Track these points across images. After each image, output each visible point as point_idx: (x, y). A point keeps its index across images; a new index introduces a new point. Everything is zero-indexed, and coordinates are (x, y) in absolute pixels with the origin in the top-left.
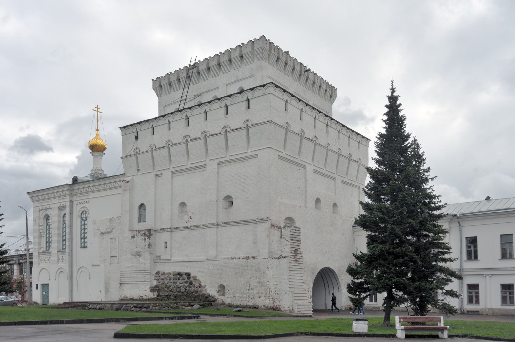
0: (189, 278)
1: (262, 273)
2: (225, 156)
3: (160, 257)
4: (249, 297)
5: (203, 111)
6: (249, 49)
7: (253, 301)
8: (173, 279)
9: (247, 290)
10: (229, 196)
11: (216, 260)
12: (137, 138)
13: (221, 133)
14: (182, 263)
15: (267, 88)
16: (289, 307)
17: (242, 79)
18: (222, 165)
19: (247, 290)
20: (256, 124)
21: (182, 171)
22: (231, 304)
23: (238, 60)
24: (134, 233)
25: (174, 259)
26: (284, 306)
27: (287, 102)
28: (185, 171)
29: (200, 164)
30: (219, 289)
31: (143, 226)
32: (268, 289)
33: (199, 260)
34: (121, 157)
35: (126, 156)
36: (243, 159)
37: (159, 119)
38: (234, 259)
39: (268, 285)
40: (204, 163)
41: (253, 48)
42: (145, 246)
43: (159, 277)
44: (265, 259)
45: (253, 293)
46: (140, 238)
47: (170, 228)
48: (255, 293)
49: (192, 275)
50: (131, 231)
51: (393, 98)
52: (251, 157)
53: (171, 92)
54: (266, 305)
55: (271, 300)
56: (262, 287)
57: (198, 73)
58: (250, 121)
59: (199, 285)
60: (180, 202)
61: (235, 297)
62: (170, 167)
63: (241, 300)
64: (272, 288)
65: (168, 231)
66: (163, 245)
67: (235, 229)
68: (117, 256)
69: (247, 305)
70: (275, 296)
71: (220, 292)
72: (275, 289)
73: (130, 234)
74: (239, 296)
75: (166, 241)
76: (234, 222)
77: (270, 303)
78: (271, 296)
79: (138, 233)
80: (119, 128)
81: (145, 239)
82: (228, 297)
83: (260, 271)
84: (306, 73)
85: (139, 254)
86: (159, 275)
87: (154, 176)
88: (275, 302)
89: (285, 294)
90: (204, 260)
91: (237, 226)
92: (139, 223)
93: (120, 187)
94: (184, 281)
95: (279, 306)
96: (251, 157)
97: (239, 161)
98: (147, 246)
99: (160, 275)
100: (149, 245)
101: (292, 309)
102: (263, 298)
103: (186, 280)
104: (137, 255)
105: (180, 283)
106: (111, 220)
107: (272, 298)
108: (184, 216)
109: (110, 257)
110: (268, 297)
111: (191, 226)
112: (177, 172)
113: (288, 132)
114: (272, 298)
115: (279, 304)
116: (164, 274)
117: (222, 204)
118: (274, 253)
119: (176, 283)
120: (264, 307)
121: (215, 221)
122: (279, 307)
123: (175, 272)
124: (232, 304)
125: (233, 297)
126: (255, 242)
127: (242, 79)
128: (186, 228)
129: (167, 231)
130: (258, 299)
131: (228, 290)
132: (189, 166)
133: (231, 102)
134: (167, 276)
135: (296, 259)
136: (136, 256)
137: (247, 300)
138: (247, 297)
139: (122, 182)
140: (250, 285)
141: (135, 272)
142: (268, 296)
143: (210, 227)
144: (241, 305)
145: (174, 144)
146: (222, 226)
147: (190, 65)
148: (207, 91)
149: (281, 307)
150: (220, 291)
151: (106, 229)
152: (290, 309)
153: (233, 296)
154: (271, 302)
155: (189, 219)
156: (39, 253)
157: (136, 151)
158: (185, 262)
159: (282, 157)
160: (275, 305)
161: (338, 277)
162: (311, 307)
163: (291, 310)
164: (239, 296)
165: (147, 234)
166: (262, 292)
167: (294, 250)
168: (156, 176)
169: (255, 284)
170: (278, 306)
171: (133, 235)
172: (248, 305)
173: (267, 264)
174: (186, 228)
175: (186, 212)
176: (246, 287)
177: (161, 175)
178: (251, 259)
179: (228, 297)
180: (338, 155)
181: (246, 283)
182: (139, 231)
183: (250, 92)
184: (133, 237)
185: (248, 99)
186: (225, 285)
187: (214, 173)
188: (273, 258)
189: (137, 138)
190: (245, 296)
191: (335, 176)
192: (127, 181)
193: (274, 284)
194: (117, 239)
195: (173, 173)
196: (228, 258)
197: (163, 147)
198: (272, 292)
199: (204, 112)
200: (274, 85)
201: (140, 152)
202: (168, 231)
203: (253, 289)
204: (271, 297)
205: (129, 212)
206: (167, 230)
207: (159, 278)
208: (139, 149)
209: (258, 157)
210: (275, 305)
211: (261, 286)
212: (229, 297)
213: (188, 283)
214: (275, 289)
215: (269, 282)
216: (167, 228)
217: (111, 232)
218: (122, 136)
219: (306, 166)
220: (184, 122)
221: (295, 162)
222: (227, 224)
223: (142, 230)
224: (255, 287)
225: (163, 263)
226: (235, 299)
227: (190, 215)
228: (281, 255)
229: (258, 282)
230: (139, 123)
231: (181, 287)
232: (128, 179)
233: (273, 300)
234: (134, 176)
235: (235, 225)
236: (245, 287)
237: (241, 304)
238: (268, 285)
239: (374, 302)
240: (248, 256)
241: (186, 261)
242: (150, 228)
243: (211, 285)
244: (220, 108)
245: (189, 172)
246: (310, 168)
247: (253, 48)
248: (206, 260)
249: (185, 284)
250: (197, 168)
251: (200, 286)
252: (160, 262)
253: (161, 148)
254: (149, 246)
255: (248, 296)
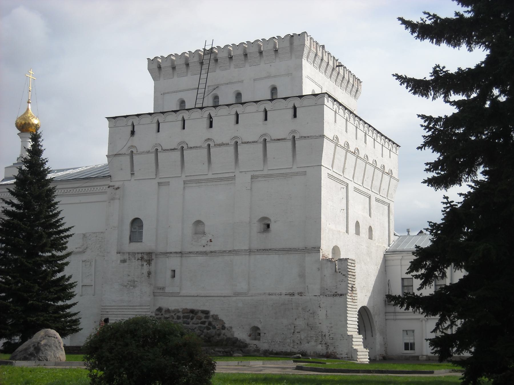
0: (207, 317)
1: (311, 313)
2: (291, 167)
3: (163, 288)
4: (293, 342)
5: (291, 106)
6: (287, 44)
7: (299, 347)
8: (183, 318)
9: (290, 333)
10: (266, 217)
11: (247, 295)
12: (133, 133)
13: (259, 141)
14: (196, 298)
15: (319, 98)
16: (347, 354)
17: (275, 76)
18: (256, 180)
19: (290, 333)
20: (305, 137)
21: (199, 181)
22: (269, 350)
23: (271, 54)
24: (126, 257)
25: (183, 292)
26: (341, 352)
27: (366, 133)
28: (204, 182)
29: (227, 175)
30: (250, 332)
31: (136, 247)
32: (319, 332)
33: (223, 295)
34: (106, 155)
35: (116, 155)
36: (285, 175)
37: (168, 114)
38: (273, 295)
39: (320, 328)
40: (232, 175)
41: (291, 44)
42: (143, 273)
43: (162, 315)
44: (316, 296)
45: (299, 337)
46: (136, 263)
47: (180, 253)
48: (303, 337)
49: (212, 313)
50: (121, 254)
51: (399, 77)
52: (297, 174)
53: (173, 77)
54: (318, 352)
55: (324, 345)
56: (312, 329)
57: (216, 60)
58: (298, 133)
59: (221, 326)
60: (195, 220)
61: (273, 341)
62: (181, 175)
63: (283, 346)
64: (325, 331)
65: (178, 256)
66: (169, 274)
67: (274, 258)
68: (92, 285)
69: (290, 352)
70: (329, 341)
71: (251, 336)
72: (329, 332)
73: (120, 257)
74: (280, 341)
75: (173, 269)
76: (273, 250)
77: (322, 350)
78: (323, 341)
79: (131, 257)
80: (106, 118)
81: (143, 265)
82: (264, 343)
83: (309, 310)
84: (337, 68)
85: (133, 284)
86: (161, 312)
87: (157, 184)
88: (329, 348)
89: (342, 339)
90: (230, 295)
91: (277, 255)
92: (131, 243)
93: (105, 193)
94: (200, 321)
95: (334, 352)
96: (297, 174)
97: (280, 177)
98: (146, 274)
99: (163, 312)
100: (149, 273)
101: (350, 357)
102: (313, 343)
103: (203, 320)
104: (129, 286)
105: (193, 324)
106: (84, 235)
107: (325, 344)
108: (201, 238)
109: (81, 287)
110: (320, 342)
111: (211, 252)
112: (191, 181)
113: (337, 146)
114: (325, 344)
115: (334, 351)
116: (168, 311)
117: (256, 227)
118: (327, 289)
119: (188, 324)
120: (314, 355)
121: (246, 248)
122: (335, 354)
123: (186, 309)
124: (270, 350)
125: (271, 342)
126: (302, 276)
127: (275, 76)
128: (205, 253)
129: (175, 256)
130: (307, 345)
131: (265, 334)
132: (210, 176)
133: (272, 108)
134: (173, 314)
135: (352, 297)
136: (128, 287)
137: (292, 345)
138: (292, 342)
139: (108, 187)
140: (296, 328)
141: (125, 307)
142: (320, 340)
143: (240, 254)
144: (282, 352)
145: (191, 148)
146: (257, 254)
147: (205, 49)
148: (227, 83)
149: (337, 354)
150: (252, 335)
151: (76, 248)
152: (348, 356)
153: (272, 341)
154: (324, 347)
155: (208, 242)
156: (153, 292)
157: (132, 150)
158: (202, 297)
159: (330, 175)
160: (329, 352)
161: (372, 318)
162: (367, 353)
163: (349, 357)
164: (280, 341)
165: (145, 258)
166: (311, 335)
167: (351, 286)
168: (159, 184)
169: (302, 326)
170: (333, 353)
171: (123, 259)
172: (292, 351)
173: (319, 303)
174: (205, 253)
175: (204, 233)
176: (290, 330)
177: (168, 184)
178: (297, 296)
179: (264, 343)
180: (356, 157)
181: (290, 325)
182: (134, 254)
183: (298, 99)
184: (124, 261)
185: (266, 110)
186: (260, 326)
187: (85, 257)
188: (326, 296)
189: (133, 133)
190: (288, 340)
191: (370, 192)
192: (116, 187)
193: (327, 327)
194: (93, 263)
195: (185, 182)
196: (265, 293)
197: (173, 150)
198: (325, 336)
199: (234, 114)
200: (328, 96)
201: (137, 152)
202: (178, 256)
203: (299, 332)
204: (323, 342)
205: (118, 228)
206: (175, 254)
207: (161, 316)
208: (136, 147)
209: (306, 175)
210: (329, 352)
211: (310, 329)
212: (266, 342)
213: (207, 324)
214: (329, 332)
215: (321, 323)
216: (176, 253)
217: (84, 252)
218: (109, 128)
219: (348, 184)
220: (205, 122)
221: (340, 179)
222: (263, 252)
223: (138, 253)
224: (302, 330)
225: (167, 297)
226: (274, 345)
227: (210, 237)
228: (336, 292)
229: (307, 324)
230: (138, 115)
231: (195, 328)
232: (117, 185)
233: (326, 345)
234: (124, 182)
235: (274, 253)
236: (288, 330)
237: (283, 351)
238: (320, 328)
239: (410, 350)
240: (292, 292)
241: (203, 295)
242: (151, 251)
243: (240, 327)
244: (257, 111)
245: (209, 184)
246: (351, 186)
247: (291, 44)
248: (233, 295)
249: (202, 325)
250: (221, 179)
251: (224, 328)
252: (162, 295)
253: (171, 150)
254: (148, 274)
255: (293, 341)
